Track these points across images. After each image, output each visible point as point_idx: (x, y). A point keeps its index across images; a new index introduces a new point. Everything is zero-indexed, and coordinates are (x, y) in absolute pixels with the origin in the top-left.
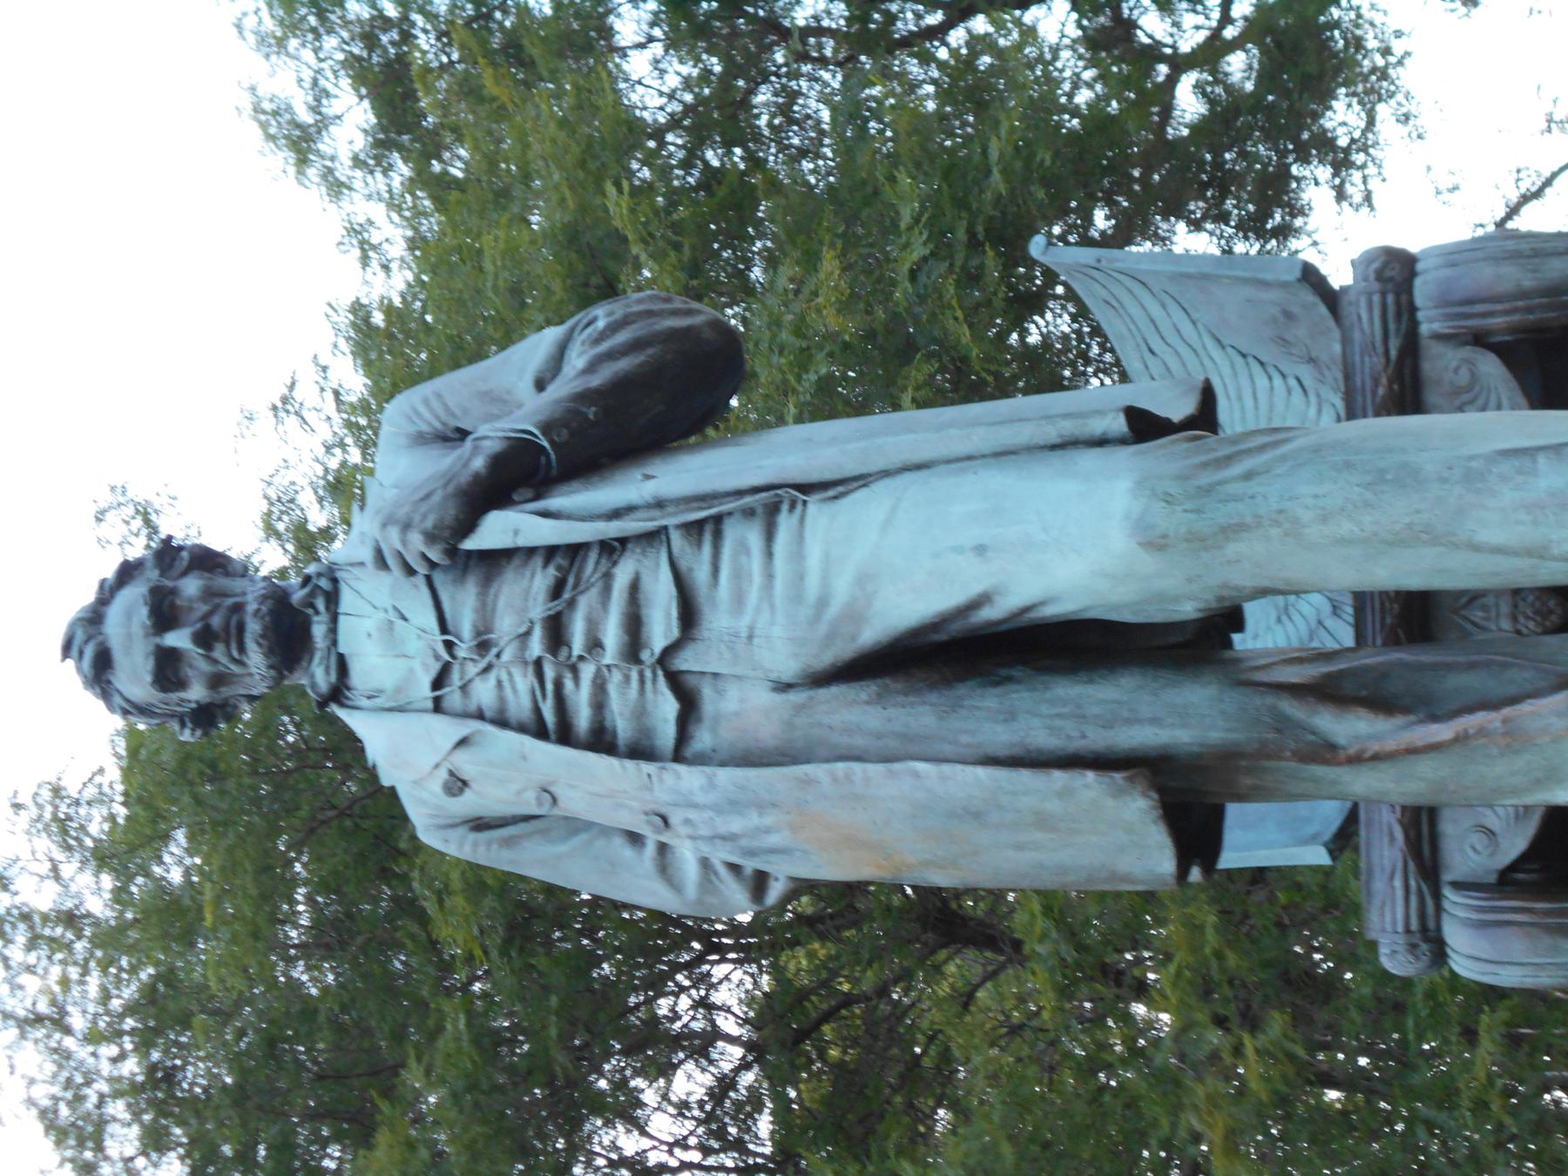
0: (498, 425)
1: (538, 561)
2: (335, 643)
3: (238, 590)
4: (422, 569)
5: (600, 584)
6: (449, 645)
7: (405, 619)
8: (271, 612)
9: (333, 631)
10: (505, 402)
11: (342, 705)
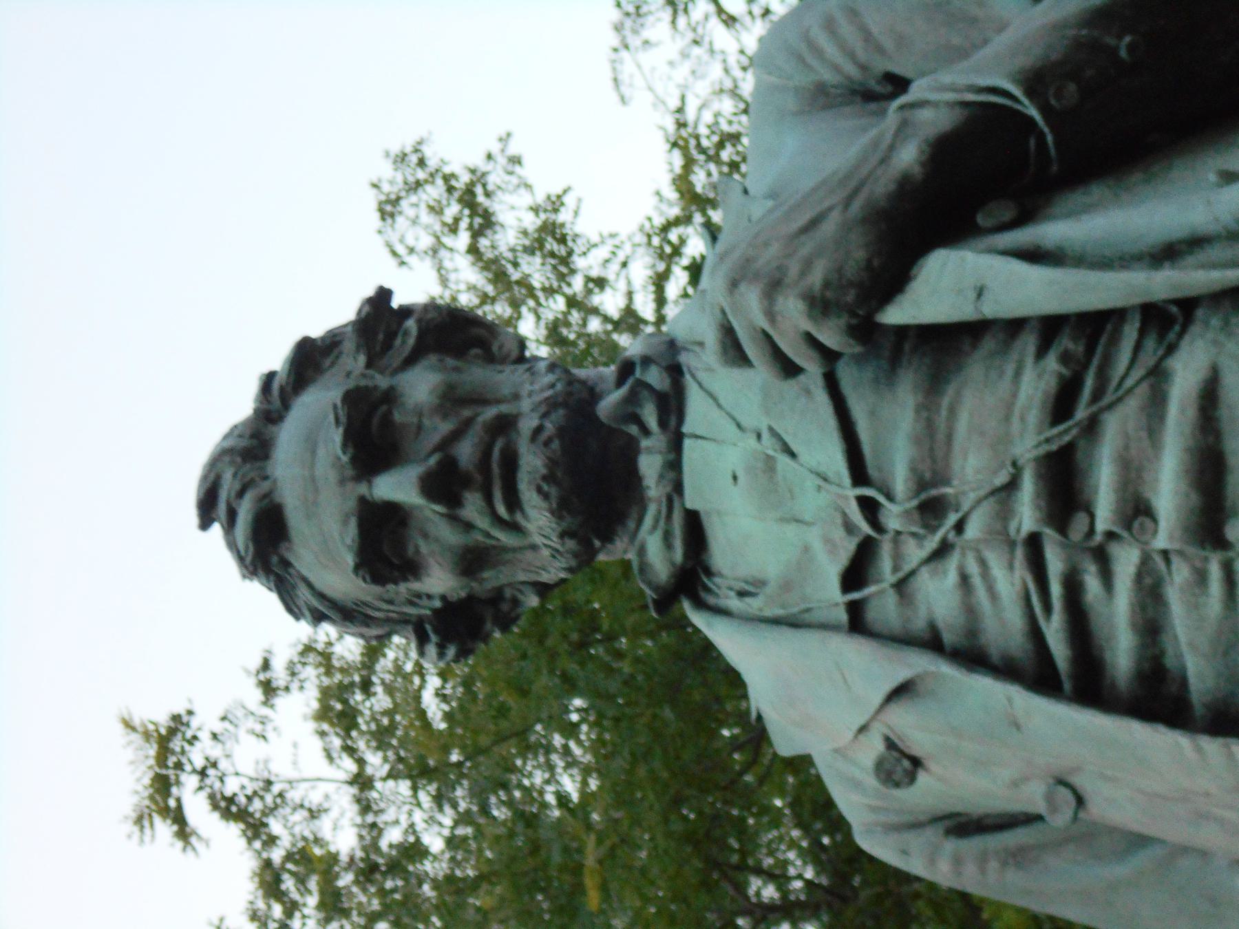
0: (946, 78)
1: (1028, 342)
2: (678, 487)
3: (506, 391)
4: (813, 369)
5: (1144, 388)
6: (869, 507)
7: (793, 455)
8: (561, 432)
9: (674, 465)
10: (974, 21)
11: (700, 605)
